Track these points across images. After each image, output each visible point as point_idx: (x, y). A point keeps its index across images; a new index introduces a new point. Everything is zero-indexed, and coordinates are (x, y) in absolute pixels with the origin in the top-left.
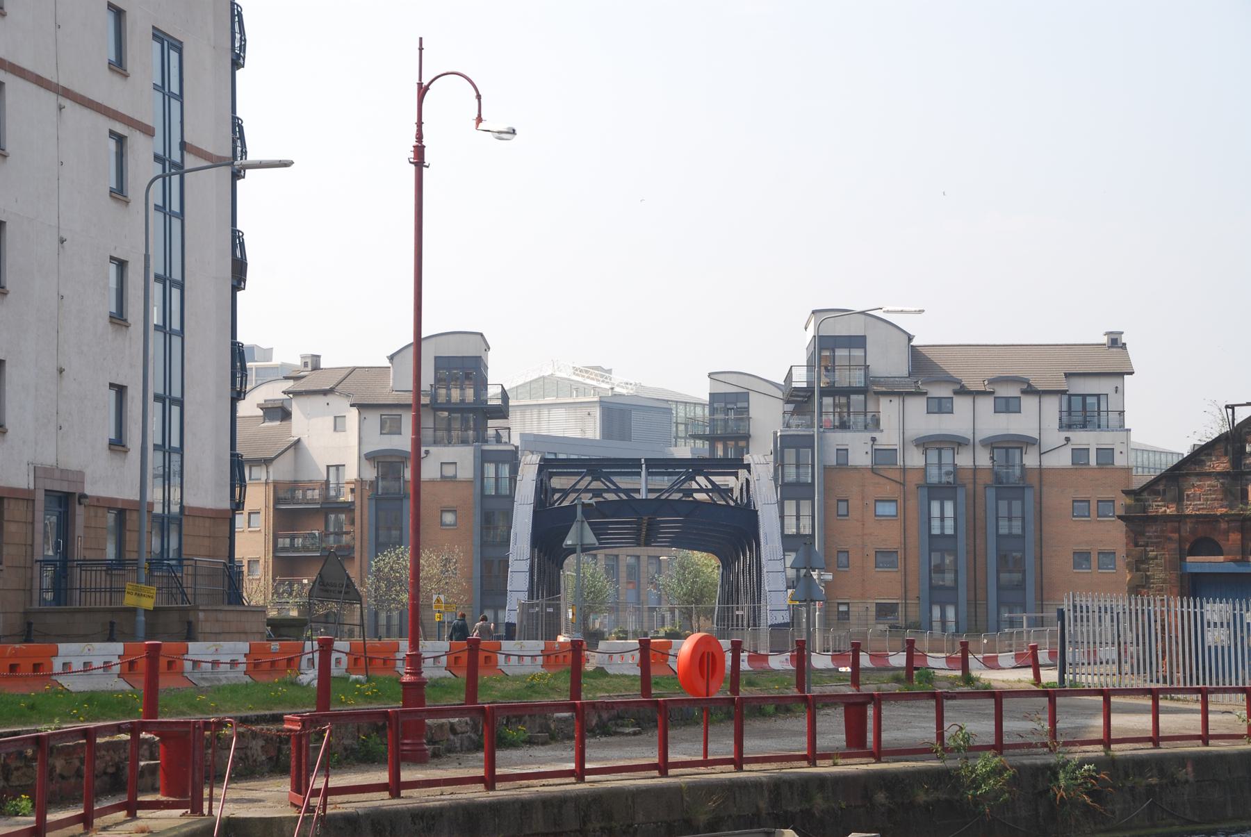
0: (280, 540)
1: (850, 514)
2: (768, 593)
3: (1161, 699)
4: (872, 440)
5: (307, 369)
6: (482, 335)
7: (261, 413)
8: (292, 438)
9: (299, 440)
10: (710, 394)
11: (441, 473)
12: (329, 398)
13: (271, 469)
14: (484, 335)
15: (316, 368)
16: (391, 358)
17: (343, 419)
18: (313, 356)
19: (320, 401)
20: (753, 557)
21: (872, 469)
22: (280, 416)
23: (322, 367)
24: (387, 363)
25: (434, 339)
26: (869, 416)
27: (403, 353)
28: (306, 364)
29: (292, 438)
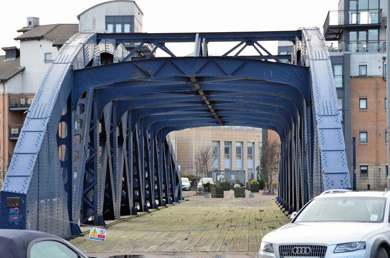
0: (12, 130)
1: (44, 55)
2: (322, 154)
3: (132, 28)
4: (383, 59)
5: (30, 26)
6: (134, 2)
7: (4, 53)
8: (20, 68)
9: (24, 69)
10: (278, 47)
11: (344, 93)
12: (42, 42)
13: (6, 86)
14: (136, 2)
15: (36, 26)
16: (79, 17)
17: (50, 55)
18: (34, 18)
19: (36, 43)
20: (304, 122)
21: (383, 77)
22: (15, 55)
23: (40, 25)
24: (77, 22)
25: (105, 5)
26: (381, 43)
27: (87, 13)
28: (30, 23)
29: (20, 68)
